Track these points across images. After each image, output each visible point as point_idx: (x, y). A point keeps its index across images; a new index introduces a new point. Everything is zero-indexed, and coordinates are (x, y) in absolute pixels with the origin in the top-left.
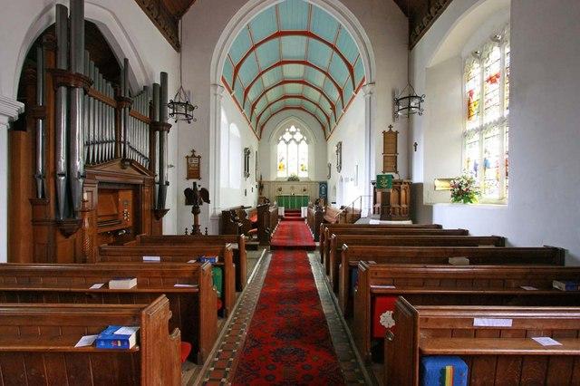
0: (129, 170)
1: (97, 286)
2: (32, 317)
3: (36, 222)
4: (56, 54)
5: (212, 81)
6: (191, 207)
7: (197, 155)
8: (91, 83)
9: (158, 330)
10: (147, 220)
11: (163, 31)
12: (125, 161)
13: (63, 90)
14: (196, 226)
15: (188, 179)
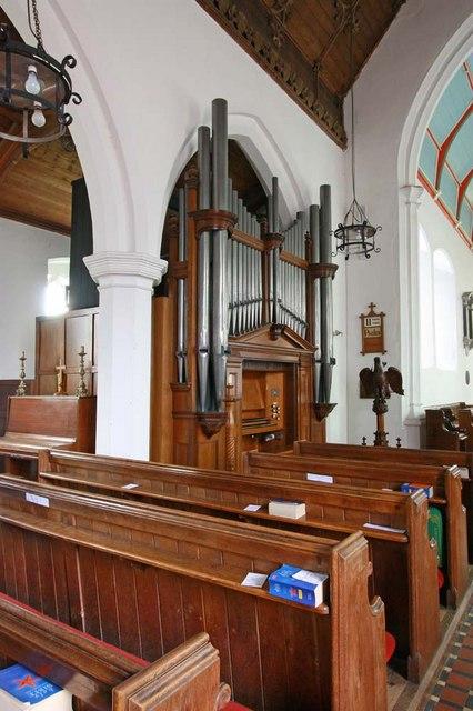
0: (282, 342)
1: (253, 509)
2: (193, 532)
3: (176, 414)
4: (198, 193)
5: (401, 180)
6: (370, 402)
7: (377, 311)
8: (235, 221)
9: (355, 588)
10: (304, 419)
11: (322, 122)
12: (276, 330)
13: (206, 235)
14: (380, 435)
15: (363, 353)
